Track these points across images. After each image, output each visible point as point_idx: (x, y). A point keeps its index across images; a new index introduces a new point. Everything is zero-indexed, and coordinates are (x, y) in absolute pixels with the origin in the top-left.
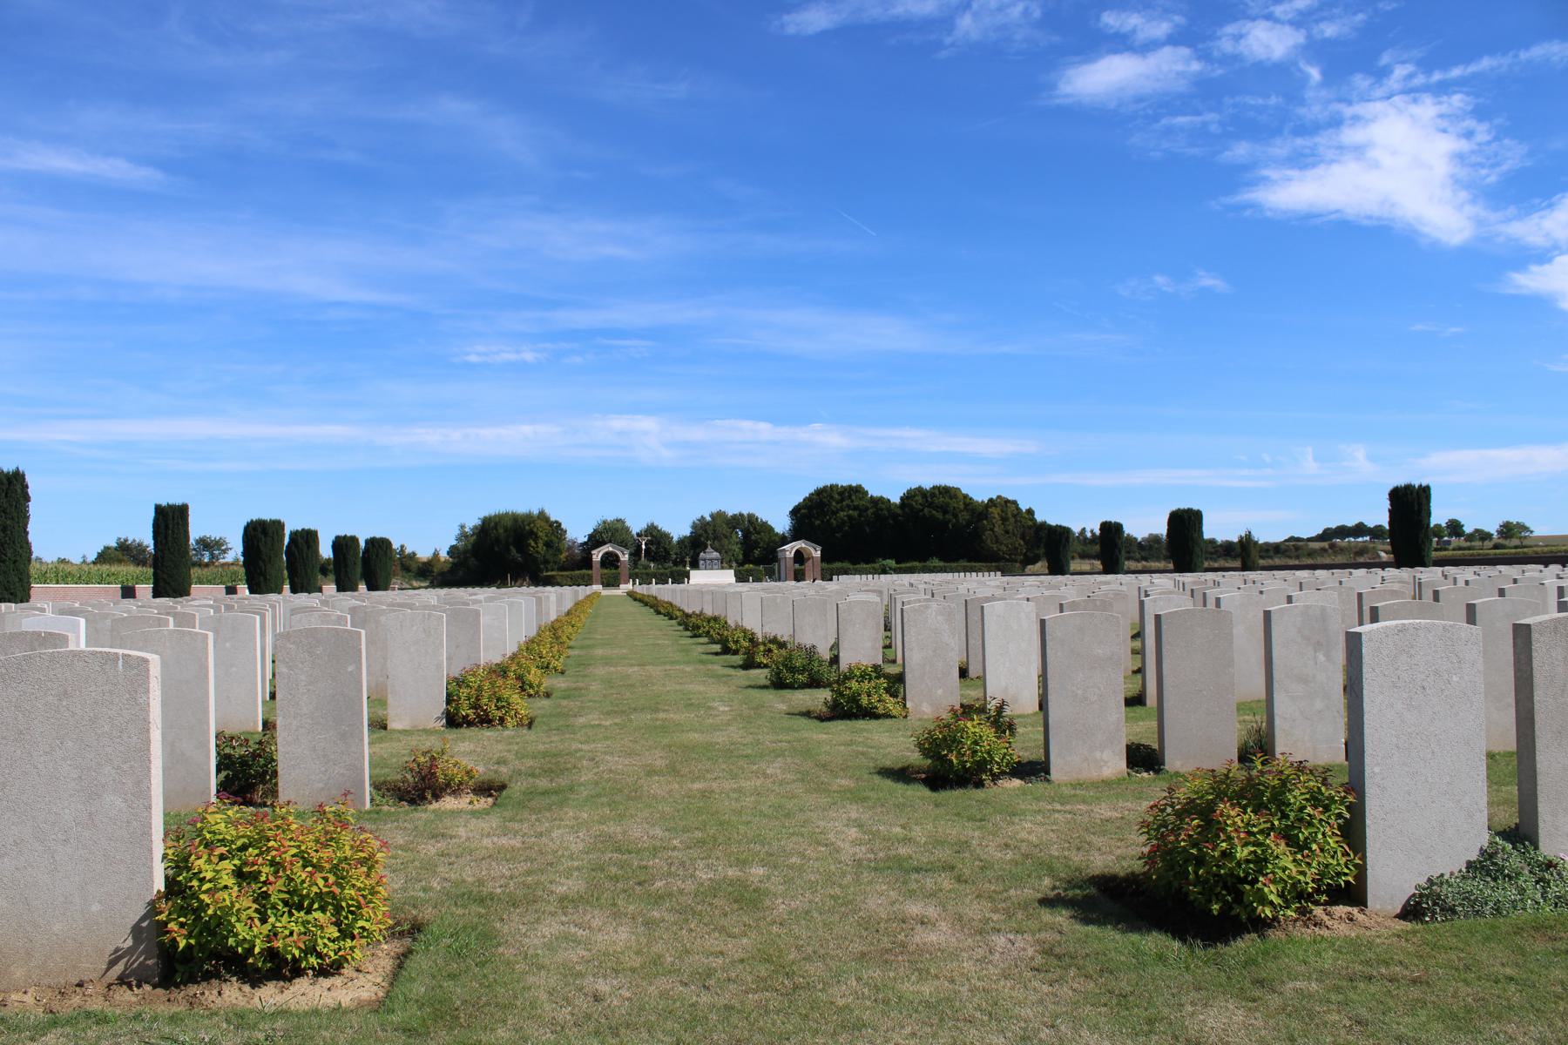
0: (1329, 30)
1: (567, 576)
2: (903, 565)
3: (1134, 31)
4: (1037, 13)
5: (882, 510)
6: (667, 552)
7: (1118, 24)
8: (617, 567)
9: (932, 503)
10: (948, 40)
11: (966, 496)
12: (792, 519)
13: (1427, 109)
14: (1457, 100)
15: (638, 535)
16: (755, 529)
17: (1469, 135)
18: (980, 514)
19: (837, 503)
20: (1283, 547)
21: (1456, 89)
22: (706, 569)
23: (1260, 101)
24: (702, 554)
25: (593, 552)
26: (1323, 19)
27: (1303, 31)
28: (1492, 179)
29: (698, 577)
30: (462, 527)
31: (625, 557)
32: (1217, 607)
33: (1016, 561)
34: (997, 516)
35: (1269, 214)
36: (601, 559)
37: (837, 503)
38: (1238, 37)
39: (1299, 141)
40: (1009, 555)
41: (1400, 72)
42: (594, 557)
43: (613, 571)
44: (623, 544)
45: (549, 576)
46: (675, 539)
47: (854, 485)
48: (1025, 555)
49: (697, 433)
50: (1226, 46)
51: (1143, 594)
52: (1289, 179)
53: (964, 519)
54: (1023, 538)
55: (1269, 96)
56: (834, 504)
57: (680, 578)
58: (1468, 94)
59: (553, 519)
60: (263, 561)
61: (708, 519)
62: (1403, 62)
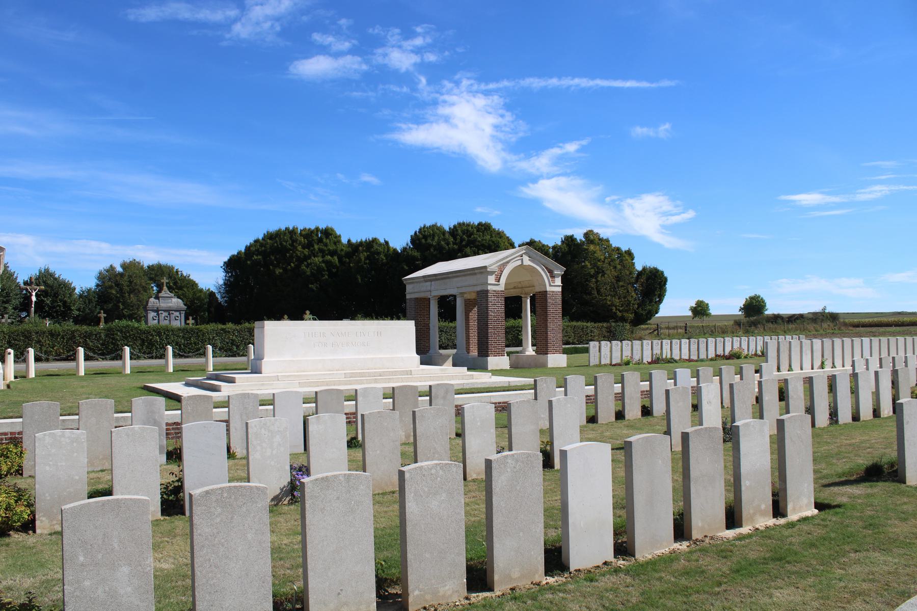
0: (431, 58)
3: (330, 45)
5: (379, 253)
10: (228, 36)
13: (480, 101)
15: (26, 283)
17: (502, 116)
21: (495, 93)
26: (429, 52)
27: (419, 55)
32: (741, 380)
37: (304, 248)
38: (385, 55)
39: (417, 112)
41: (465, 83)
46: (77, 291)
47: (322, 226)
50: (380, 60)
52: (411, 129)
55: (402, 87)
56: (299, 248)
58: (501, 97)
61: (119, 269)
62: (468, 78)
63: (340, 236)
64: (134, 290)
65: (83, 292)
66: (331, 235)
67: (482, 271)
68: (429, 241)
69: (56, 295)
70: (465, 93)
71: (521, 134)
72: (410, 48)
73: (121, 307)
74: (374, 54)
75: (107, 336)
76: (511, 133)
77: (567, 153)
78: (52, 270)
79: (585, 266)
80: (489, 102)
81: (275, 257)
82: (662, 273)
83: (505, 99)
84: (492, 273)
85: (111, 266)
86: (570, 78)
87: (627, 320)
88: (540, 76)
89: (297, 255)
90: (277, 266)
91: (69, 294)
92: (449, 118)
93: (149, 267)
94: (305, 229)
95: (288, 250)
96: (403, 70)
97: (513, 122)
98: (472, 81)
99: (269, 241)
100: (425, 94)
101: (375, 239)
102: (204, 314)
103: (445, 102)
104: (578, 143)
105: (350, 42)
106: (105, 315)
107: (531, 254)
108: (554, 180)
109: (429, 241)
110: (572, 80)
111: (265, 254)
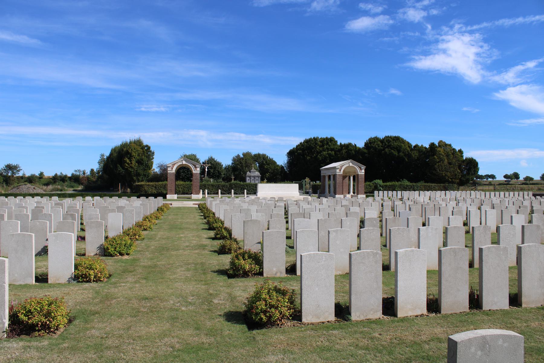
0: (434, 12)
1: (153, 186)
2: (388, 184)
3: (370, 10)
4: (338, 3)
5: (351, 150)
6: (220, 173)
7: (365, 7)
8: (191, 181)
10: (309, 10)
12: (288, 157)
13: (467, 38)
14: (477, 35)
15: (203, 163)
16: (266, 162)
17: (481, 47)
19: (320, 147)
21: (477, 32)
23: (413, 34)
27: (426, 11)
28: (489, 62)
30: (102, 155)
35: (415, 70)
37: (320, 147)
38: (404, 13)
39: (425, 47)
40: (451, 179)
41: (457, 26)
43: (188, 183)
45: (139, 185)
46: (224, 166)
47: (329, 137)
48: (460, 179)
49: (220, 137)
50: (401, 16)
51: (482, 201)
52: (421, 59)
56: (318, 147)
58: (481, 34)
59: (145, 143)
61: (242, 156)
62: (459, 23)
63: (337, 141)
64: (248, 166)
65: (226, 166)
66: (333, 141)
67: (334, 168)
68: (372, 145)
69: (215, 168)
70: (457, 34)
71: (494, 58)
72: (420, 7)
73: (242, 173)
74: (398, 13)
75: (229, 186)
76: (487, 58)
77: (528, 69)
78: (213, 157)
79: (435, 158)
80: (472, 38)
81: (308, 152)
82: (475, 160)
83: (484, 35)
84: (338, 169)
85: (238, 155)
86: (532, 16)
87: (455, 183)
88: (510, 17)
89: (317, 151)
91: (221, 168)
92: (446, 51)
93: (254, 155)
94: (321, 138)
95: (313, 148)
96: (417, 21)
97: (488, 50)
98: (462, 25)
99: (305, 144)
100: (430, 36)
101: (350, 143)
102: (279, 177)
103: (443, 40)
104: (536, 61)
105: (382, 7)
106: (234, 177)
107: (352, 162)
108: (518, 87)
109: (372, 145)
110: (534, 17)
111: (303, 150)
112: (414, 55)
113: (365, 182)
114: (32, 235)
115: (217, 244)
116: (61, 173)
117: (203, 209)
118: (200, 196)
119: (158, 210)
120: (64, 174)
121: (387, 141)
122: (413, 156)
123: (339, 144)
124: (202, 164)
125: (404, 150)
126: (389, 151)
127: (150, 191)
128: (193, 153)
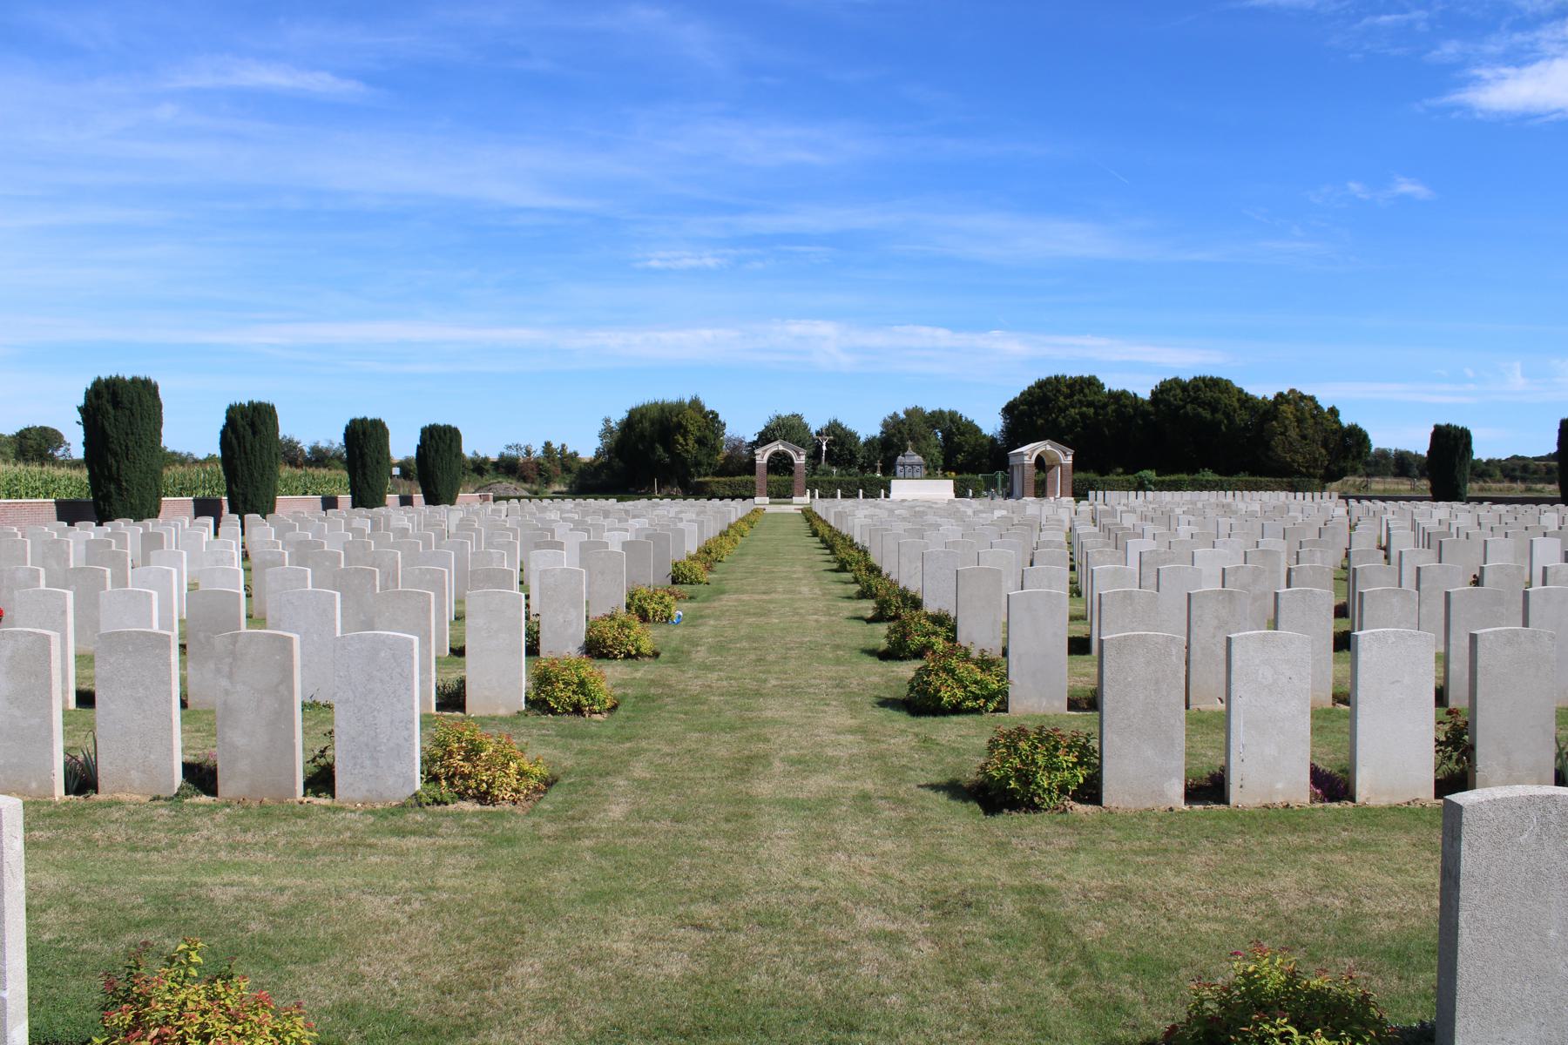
2: (1167, 478)
5: (1126, 407)
8: (791, 473)
9: (1196, 398)
11: (1240, 391)
12: (1005, 418)
15: (818, 433)
16: (958, 429)
18: (1266, 412)
19: (1066, 398)
20: (1532, 466)
22: (905, 478)
24: (900, 457)
25: (757, 452)
29: (901, 489)
30: (607, 421)
31: (800, 460)
33: (1315, 477)
34: (1290, 416)
35: (1479, 116)
36: (769, 461)
37: (1066, 398)
39: (1518, 37)
42: (758, 458)
44: (800, 443)
45: (701, 482)
47: (1086, 375)
48: (1327, 468)
49: (877, 339)
52: (1503, 78)
53: (1243, 420)
54: (1325, 445)
56: (1061, 398)
57: (877, 490)
59: (708, 408)
60: (115, 454)
61: (902, 416)
67: (1021, 453)
69: (843, 444)
79: (1273, 426)
89: (1059, 407)
90: (1039, 417)
95: (1051, 401)
112: (1478, 65)
113: (1073, 472)
114: (291, 639)
115: (880, 635)
116: (475, 453)
117: (809, 515)
118: (807, 499)
119: (720, 535)
120: (482, 455)
121: (1193, 388)
122: (1237, 419)
123: (1106, 390)
124: (815, 435)
125: (1226, 406)
126: (1194, 409)
127: (721, 492)
128: (796, 413)
